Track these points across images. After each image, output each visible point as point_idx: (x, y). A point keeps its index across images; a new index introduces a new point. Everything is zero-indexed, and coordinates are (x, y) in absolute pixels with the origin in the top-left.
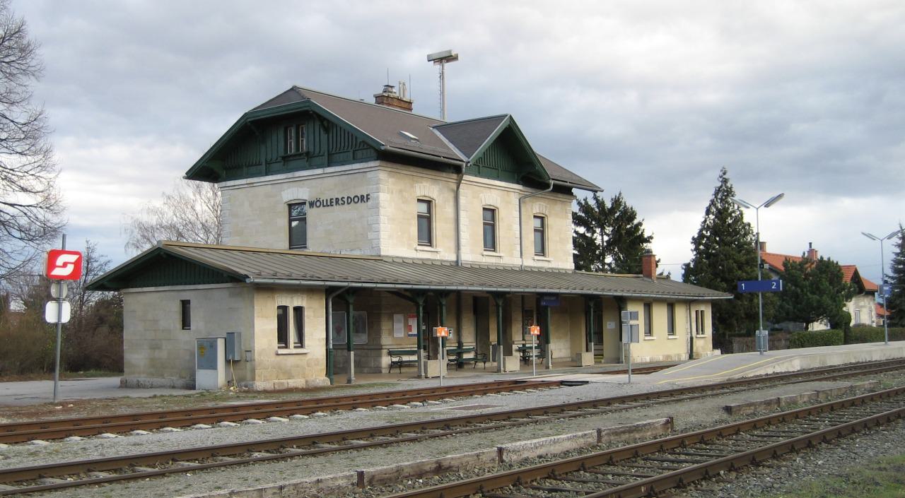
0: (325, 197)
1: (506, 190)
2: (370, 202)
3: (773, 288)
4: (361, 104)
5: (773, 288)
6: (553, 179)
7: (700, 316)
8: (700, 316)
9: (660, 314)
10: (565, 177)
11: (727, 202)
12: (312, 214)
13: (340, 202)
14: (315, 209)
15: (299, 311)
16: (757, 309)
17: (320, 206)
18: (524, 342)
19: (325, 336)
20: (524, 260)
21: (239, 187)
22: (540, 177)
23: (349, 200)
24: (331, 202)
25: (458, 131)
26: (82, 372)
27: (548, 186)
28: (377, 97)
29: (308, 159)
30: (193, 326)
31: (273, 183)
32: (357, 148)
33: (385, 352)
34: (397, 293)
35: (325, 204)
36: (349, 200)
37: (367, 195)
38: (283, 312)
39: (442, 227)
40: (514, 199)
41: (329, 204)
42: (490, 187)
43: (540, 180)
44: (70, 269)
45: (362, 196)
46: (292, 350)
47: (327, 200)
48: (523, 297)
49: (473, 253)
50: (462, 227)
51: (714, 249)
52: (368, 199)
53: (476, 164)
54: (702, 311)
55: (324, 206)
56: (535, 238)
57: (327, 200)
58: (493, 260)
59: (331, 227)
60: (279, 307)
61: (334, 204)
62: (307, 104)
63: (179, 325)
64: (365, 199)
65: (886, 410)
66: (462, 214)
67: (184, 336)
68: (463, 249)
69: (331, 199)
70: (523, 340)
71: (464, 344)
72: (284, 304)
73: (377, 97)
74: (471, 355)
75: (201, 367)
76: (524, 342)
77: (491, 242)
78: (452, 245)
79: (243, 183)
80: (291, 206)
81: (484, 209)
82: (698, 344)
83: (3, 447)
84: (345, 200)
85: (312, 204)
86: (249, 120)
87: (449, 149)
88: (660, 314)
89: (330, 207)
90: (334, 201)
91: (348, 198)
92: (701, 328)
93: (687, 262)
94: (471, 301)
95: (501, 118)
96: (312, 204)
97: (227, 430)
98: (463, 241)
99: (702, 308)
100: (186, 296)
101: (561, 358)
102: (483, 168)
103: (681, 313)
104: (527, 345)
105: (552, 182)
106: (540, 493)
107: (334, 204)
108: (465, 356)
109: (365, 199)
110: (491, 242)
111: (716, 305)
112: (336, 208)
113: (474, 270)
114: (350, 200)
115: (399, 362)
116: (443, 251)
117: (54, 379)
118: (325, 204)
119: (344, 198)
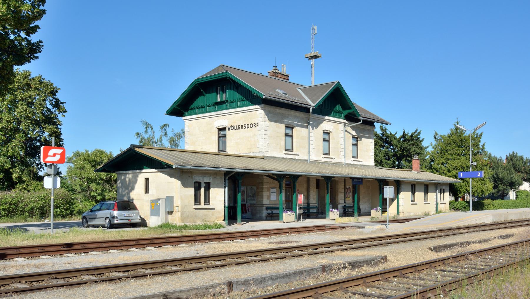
0: (236, 124)
3: (478, 176)
5: (478, 176)
6: (362, 117)
10: (371, 117)
13: (243, 127)
16: (30, 221)
18: (345, 204)
19: (223, 199)
20: (346, 160)
22: (356, 116)
23: (248, 126)
24: (239, 127)
27: (360, 120)
32: (252, 98)
33: (264, 208)
34: (269, 176)
41: (238, 128)
43: (356, 118)
44: (58, 158)
46: (202, 205)
48: (345, 179)
54: (444, 189)
59: (239, 140)
60: (195, 182)
61: (240, 128)
62: (226, 74)
64: (256, 126)
65: (527, 223)
69: (239, 126)
70: (345, 203)
71: (311, 205)
72: (208, 181)
74: (315, 210)
76: (345, 204)
80: (220, 130)
81: (324, 133)
84: (246, 126)
86: (197, 83)
87: (304, 98)
90: (240, 126)
91: (248, 125)
94: (315, 182)
101: (366, 213)
104: (347, 206)
105: (362, 119)
106: (324, 298)
107: (240, 128)
108: (311, 211)
112: (241, 130)
115: (271, 214)
117: (436, 192)
118: (236, 128)
119: (245, 125)
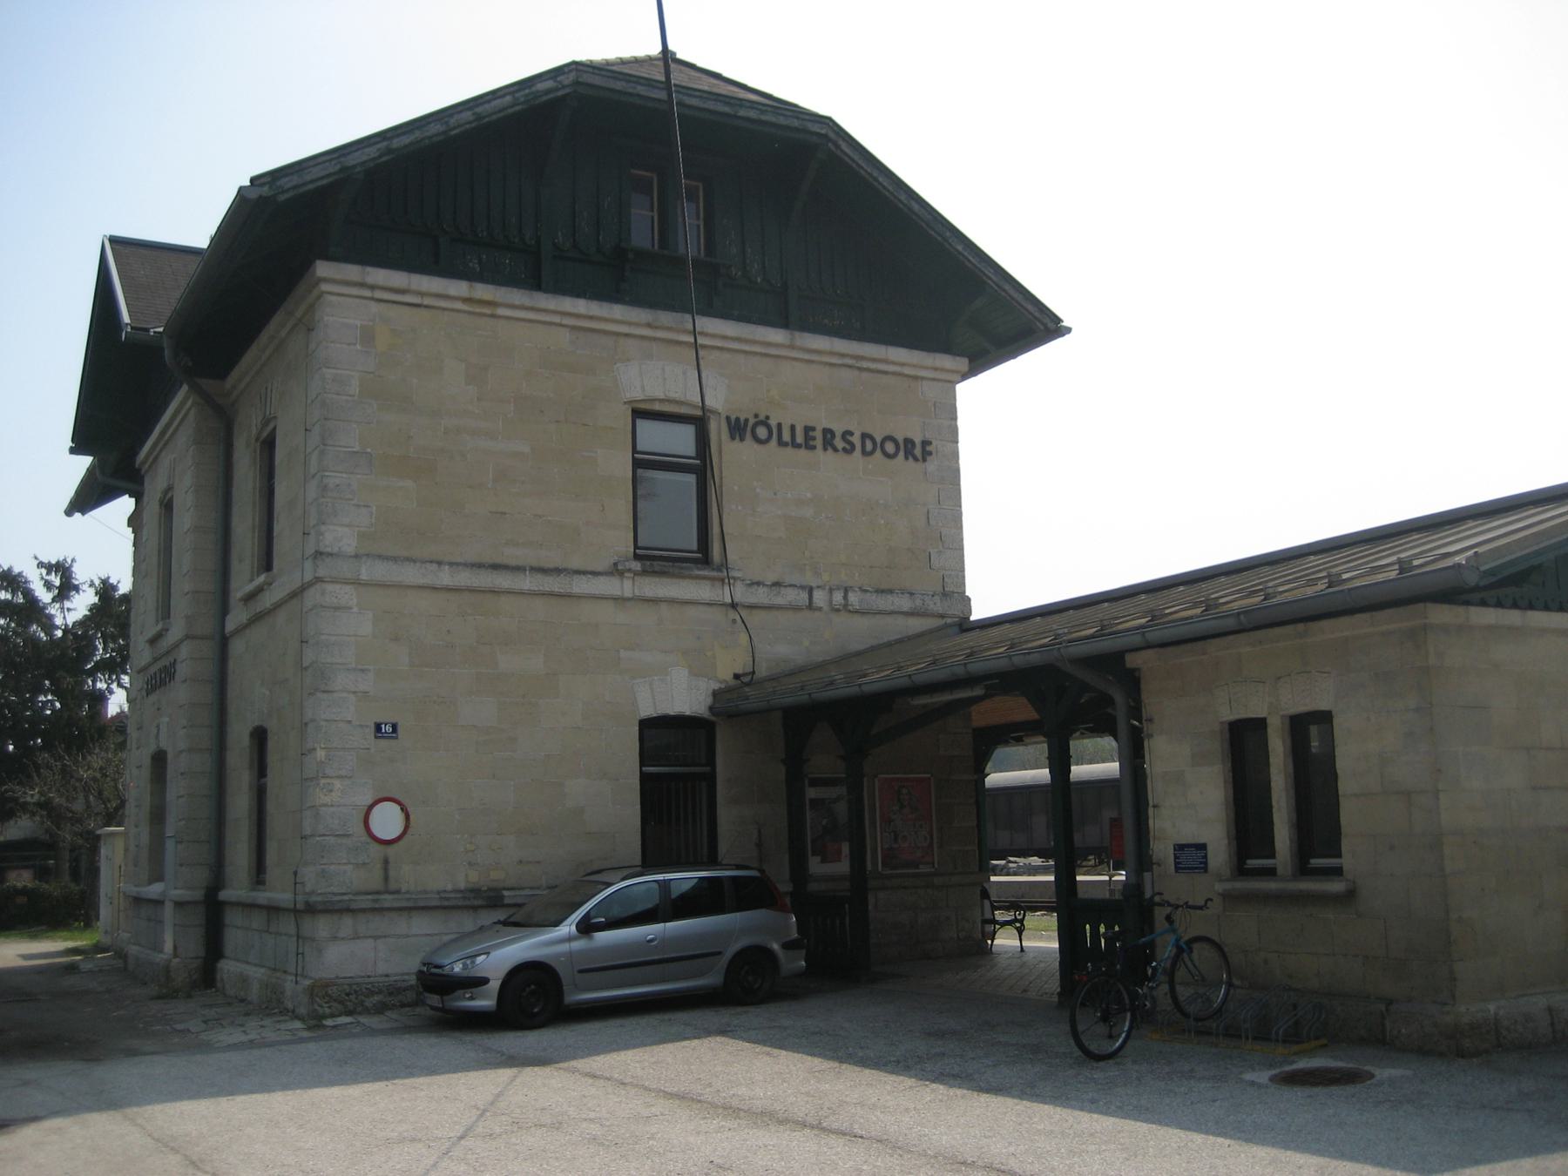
2: (932, 465)
17: (872, 452)
26: (176, 1040)
30: (1323, 706)
35: (786, 437)
36: (869, 446)
37: (925, 443)
41: (800, 439)
45: (909, 443)
47: (793, 428)
52: (926, 454)
54: (1300, 725)
55: (781, 443)
57: (793, 428)
79: (876, 356)
84: (856, 440)
89: (803, 452)
90: (818, 434)
91: (864, 436)
93: (113, 696)
97: (701, 1095)
107: (819, 442)
109: (918, 451)
114: (871, 445)
118: (786, 437)
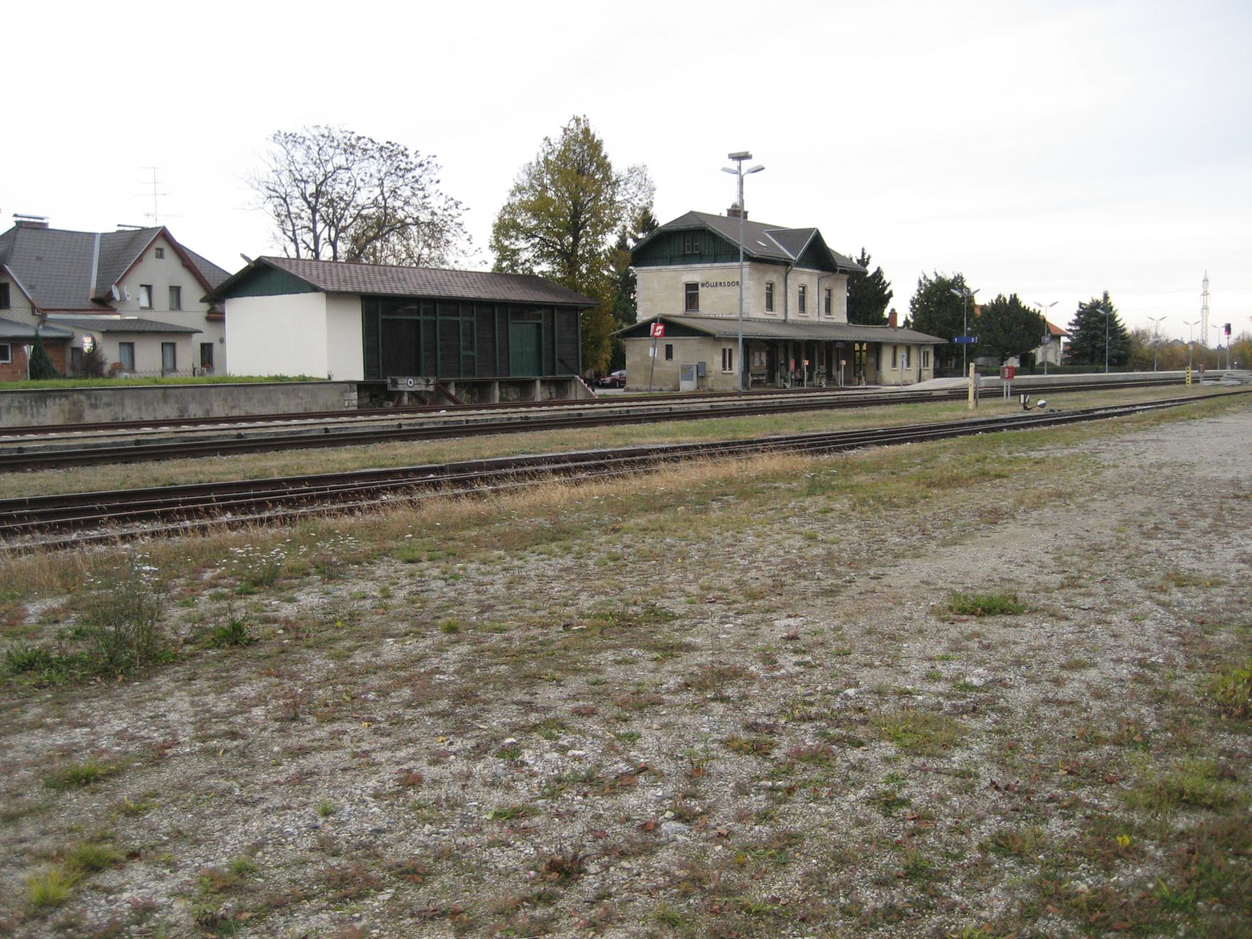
1: (811, 274)
4: (720, 217)
7: (926, 354)
8: (926, 354)
9: (901, 354)
11: (1093, 352)
12: (702, 291)
14: (705, 288)
15: (730, 350)
21: (651, 271)
25: (784, 235)
28: (729, 210)
29: (700, 258)
30: (674, 358)
31: (675, 270)
38: (760, 349)
39: (778, 299)
40: (815, 279)
42: (803, 273)
49: (794, 315)
50: (789, 299)
51: (609, 270)
53: (801, 259)
56: (465, 274)
58: (804, 319)
63: (664, 357)
66: (789, 290)
67: (668, 363)
68: (789, 313)
73: (729, 210)
75: (683, 379)
77: (802, 308)
78: (783, 309)
82: (924, 373)
83: (5, 546)
85: (703, 285)
88: (901, 354)
92: (926, 363)
95: (811, 230)
96: (703, 285)
98: (789, 308)
99: (928, 349)
100: (669, 343)
102: (804, 262)
103: (914, 354)
110: (802, 308)
111: (937, 348)
112: (720, 288)
113: (795, 325)
116: (778, 314)
